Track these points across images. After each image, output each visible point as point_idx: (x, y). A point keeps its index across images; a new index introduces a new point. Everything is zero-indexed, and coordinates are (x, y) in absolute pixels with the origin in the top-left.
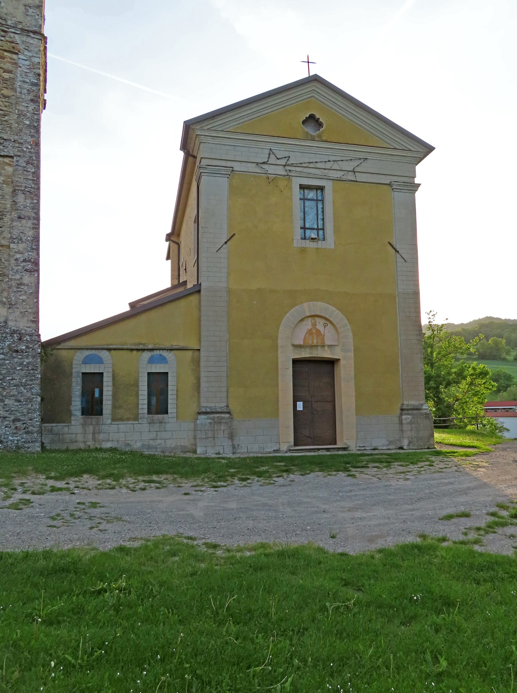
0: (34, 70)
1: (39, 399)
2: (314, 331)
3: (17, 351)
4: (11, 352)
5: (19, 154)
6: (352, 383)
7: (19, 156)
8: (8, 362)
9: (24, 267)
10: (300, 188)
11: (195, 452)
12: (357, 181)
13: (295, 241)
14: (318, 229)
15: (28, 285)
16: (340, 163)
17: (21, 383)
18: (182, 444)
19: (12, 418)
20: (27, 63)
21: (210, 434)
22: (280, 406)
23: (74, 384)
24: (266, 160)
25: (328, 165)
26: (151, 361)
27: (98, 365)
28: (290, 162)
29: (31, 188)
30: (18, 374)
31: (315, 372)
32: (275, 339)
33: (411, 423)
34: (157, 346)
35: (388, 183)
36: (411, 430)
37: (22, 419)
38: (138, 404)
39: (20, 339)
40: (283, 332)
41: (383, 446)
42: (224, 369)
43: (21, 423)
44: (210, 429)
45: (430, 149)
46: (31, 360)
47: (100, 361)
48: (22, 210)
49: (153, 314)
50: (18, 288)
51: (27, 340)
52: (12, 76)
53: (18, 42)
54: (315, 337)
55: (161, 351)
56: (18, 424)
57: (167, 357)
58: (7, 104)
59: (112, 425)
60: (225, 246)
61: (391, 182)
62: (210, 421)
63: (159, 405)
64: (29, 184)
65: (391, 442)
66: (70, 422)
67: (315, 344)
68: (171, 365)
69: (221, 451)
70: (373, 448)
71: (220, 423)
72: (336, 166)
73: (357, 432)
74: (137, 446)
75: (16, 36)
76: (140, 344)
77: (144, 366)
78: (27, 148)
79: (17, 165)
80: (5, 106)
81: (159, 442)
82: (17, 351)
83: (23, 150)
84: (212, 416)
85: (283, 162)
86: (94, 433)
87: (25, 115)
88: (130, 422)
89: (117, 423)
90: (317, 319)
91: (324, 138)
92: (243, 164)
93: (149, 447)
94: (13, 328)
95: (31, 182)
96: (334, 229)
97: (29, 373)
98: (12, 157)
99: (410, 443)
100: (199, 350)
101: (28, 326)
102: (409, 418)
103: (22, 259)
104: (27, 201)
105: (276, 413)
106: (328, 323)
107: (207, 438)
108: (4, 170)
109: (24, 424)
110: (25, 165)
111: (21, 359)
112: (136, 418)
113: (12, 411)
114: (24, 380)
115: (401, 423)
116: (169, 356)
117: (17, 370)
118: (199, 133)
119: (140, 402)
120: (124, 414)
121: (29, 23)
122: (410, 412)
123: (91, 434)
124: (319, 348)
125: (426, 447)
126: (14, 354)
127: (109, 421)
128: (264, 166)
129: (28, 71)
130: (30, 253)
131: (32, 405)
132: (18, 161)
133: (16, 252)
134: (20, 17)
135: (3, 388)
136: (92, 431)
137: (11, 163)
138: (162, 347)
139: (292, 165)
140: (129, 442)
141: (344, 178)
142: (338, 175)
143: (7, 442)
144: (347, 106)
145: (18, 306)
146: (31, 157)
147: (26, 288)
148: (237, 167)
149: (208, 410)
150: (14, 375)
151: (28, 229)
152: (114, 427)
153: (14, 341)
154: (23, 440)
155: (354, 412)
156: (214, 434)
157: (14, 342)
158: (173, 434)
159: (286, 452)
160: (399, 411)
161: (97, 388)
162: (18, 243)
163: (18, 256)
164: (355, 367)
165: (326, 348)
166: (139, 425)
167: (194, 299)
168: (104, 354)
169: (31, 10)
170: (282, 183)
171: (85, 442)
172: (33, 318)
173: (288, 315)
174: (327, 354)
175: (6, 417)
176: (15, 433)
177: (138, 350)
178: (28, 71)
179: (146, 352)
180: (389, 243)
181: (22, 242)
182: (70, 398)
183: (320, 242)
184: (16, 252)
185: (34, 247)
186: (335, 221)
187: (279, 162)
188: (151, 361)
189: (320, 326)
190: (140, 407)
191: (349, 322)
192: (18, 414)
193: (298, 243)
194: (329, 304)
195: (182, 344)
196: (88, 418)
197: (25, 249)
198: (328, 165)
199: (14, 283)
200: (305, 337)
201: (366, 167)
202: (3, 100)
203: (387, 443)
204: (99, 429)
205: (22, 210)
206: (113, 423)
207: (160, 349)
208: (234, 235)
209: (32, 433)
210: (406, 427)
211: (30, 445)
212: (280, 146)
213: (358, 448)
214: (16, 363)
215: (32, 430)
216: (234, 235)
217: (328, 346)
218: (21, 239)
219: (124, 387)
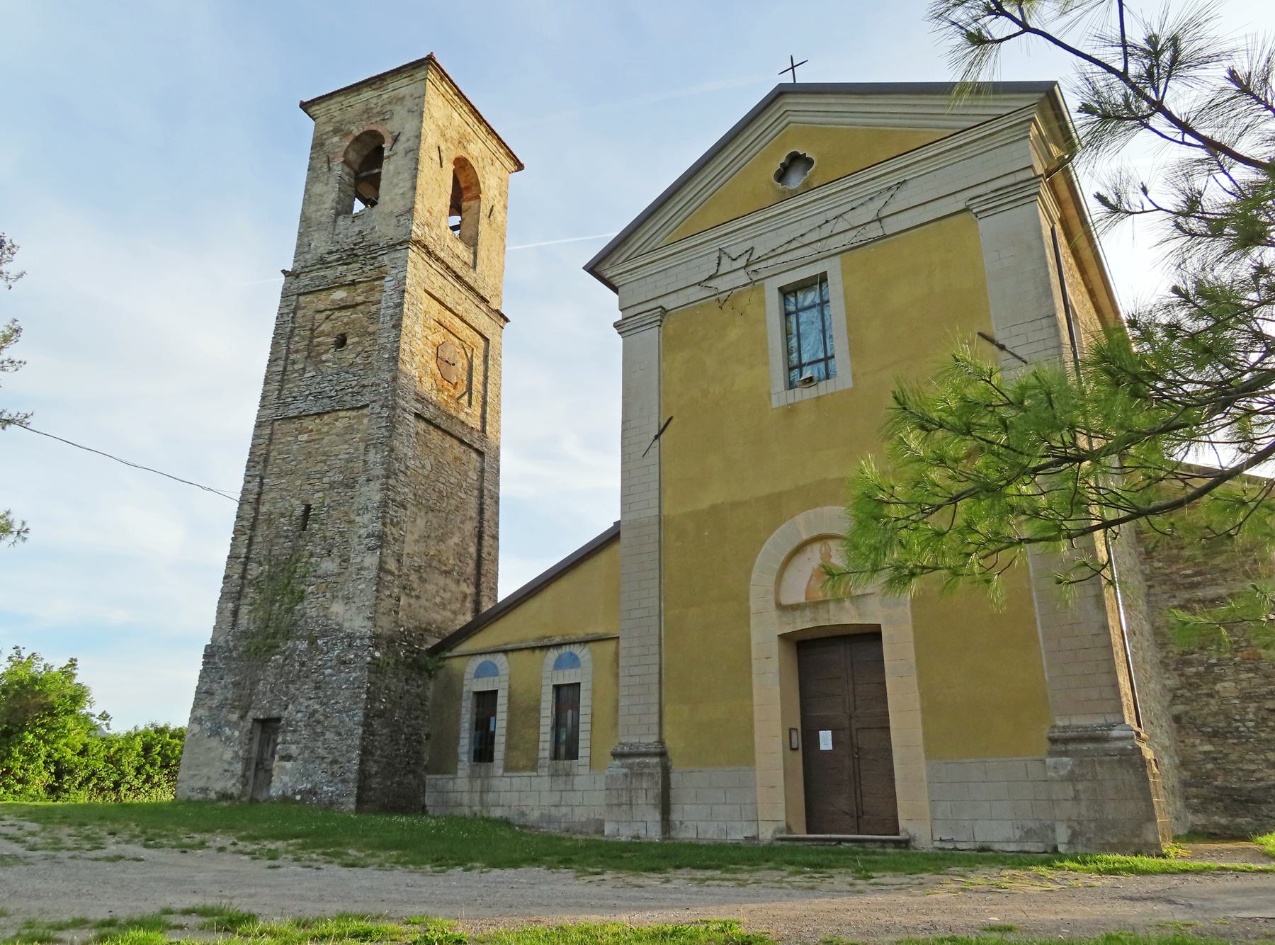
1: (360, 731)
3: (344, 663)
6: (913, 679)
13: (774, 397)
21: (624, 799)
23: (463, 711)
25: (825, 231)
26: (559, 665)
31: (833, 661)
32: (742, 599)
35: (962, 206)
36: (1076, 798)
39: (350, 645)
41: (1008, 841)
56: (336, 768)
62: (625, 770)
65: (1028, 834)
66: (456, 773)
68: (585, 670)
70: (978, 845)
71: (641, 774)
74: (534, 815)
77: (548, 673)
81: (564, 810)
82: (344, 663)
85: (742, 262)
86: (481, 792)
93: (550, 820)
96: (850, 348)
102: (1064, 765)
105: (747, 757)
107: (619, 805)
112: (534, 767)
116: (583, 653)
120: (524, 761)
122: (1071, 747)
127: (500, 772)
128: (712, 283)
138: (574, 638)
139: (759, 260)
144: (849, 104)
148: (669, 303)
149: (626, 749)
155: (921, 751)
156: (631, 798)
157: (342, 651)
158: (586, 796)
163: (362, 531)
165: (847, 604)
168: (500, 660)
173: (766, 546)
177: (542, 648)
182: (458, 732)
183: (822, 384)
186: (850, 331)
187: (737, 265)
188: (559, 665)
193: (780, 396)
195: (600, 630)
201: (904, 198)
203: (1018, 833)
207: (570, 644)
208: (670, 419)
216: (670, 419)
219: (524, 713)
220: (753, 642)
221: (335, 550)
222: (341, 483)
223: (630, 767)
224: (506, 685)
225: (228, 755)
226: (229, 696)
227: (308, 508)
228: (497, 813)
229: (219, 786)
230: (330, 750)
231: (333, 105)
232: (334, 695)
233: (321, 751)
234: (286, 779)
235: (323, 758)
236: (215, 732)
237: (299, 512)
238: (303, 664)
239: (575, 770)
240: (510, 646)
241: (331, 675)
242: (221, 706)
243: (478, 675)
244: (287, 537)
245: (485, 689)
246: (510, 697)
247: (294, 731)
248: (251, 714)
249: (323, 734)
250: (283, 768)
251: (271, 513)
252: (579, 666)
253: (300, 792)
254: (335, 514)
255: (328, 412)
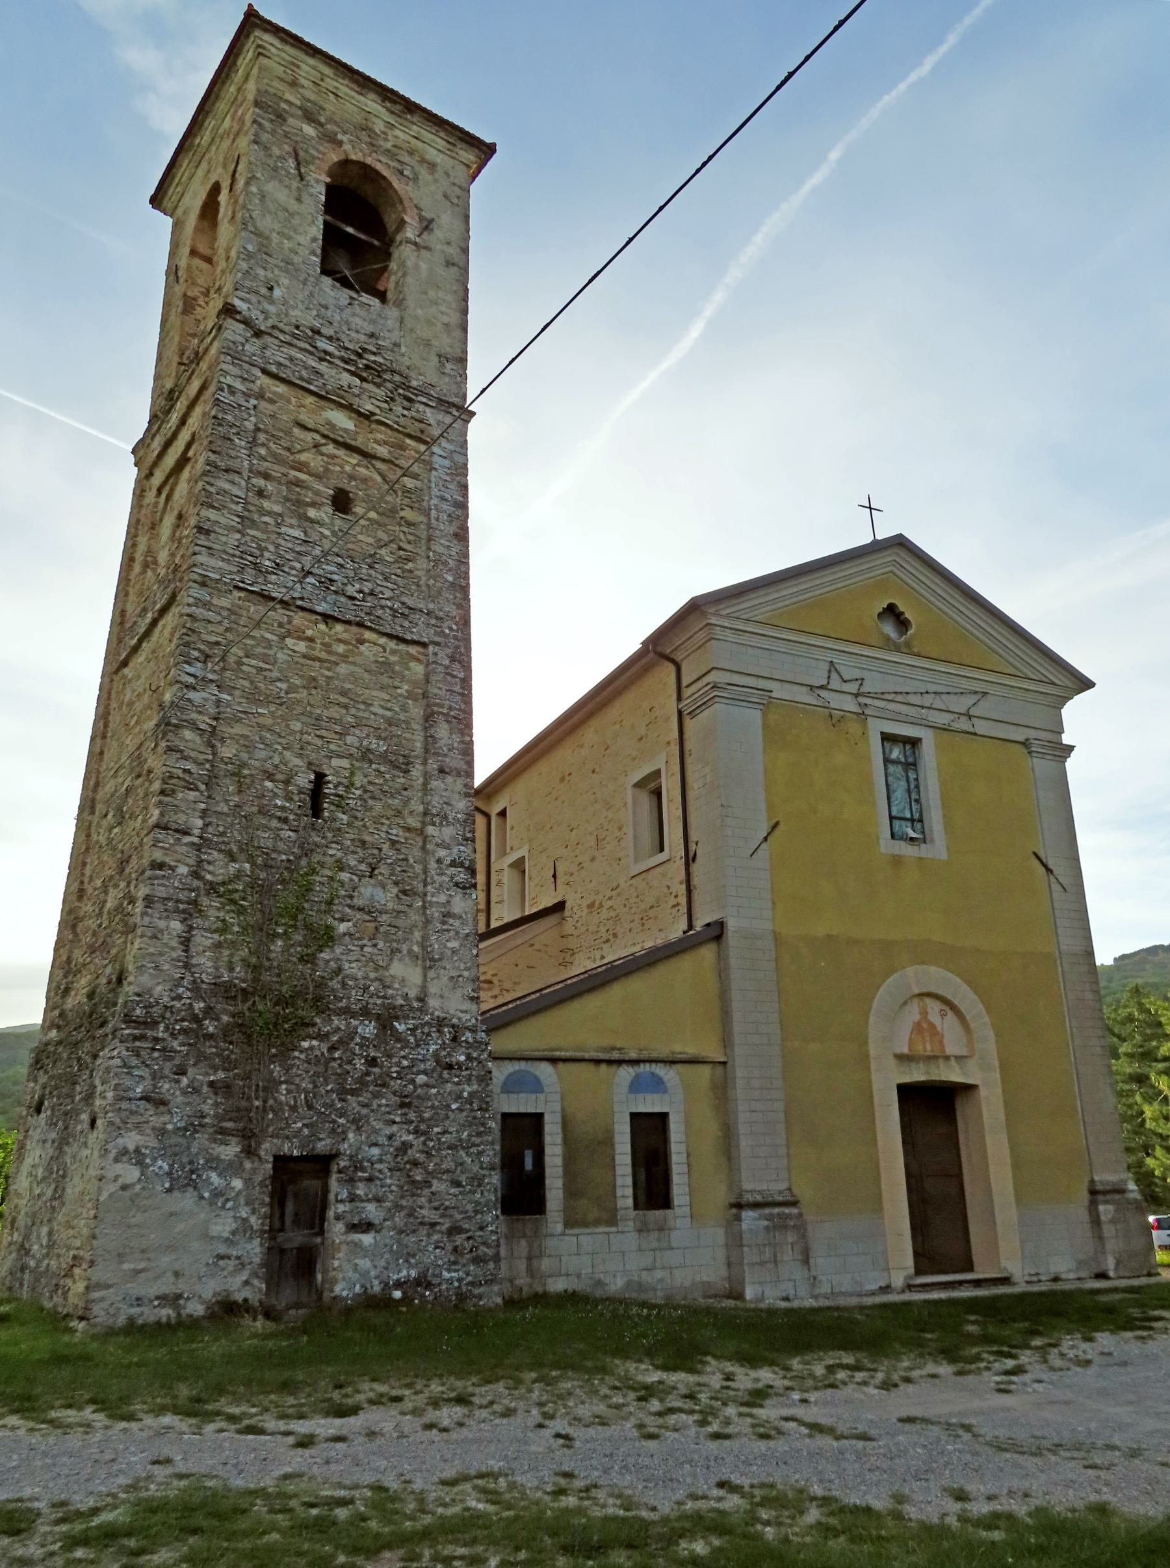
0: (458, 479)
2: (925, 1026)
4: (439, 1069)
5: (437, 639)
6: (1004, 1137)
7: (438, 644)
8: (434, 1091)
9: (452, 878)
10: (883, 740)
11: (740, 1296)
12: (975, 734)
14: (912, 820)
15: (461, 917)
16: (944, 697)
17: (460, 1140)
18: (705, 1279)
19: (447, 1226)
20: (447, 463)
21: (768, 1255)
22: (883, 1187)
24: (824, 682)
25: (927, 700)
26: (636, 1087)
27: (533, 1096)
28: (864, 689)
29: (460, 710)
30: (454, 1121)
33: (1113, 1221)
34: (645, 1055)
37: (466, 1226)
38: (614, 1186)
39: (454, 1039)
40: (875, 1031)
42: (780, 1106)
43: (464, 1236)
44: (766, 1242)
45: (1086, 684)
46: (475, 1087)
47: (536, 1086)
48: (446, 755)
49: (635, 984)
50: (444, 923)
51: (466, 1042)
52: (418, 484)
53: (432, 422)
54: (928, 1039)
55: (654, 1065)
56: (459, 1240)
57: (665, 1079)
58: (411, 538)
59: (566, 1238)
60: (764, 846)
61: (1027, 740)
63: (654, 1190)
64: (456, 703)
67: (929, 1053)
68: (677, 1099)
69: (792, 1293)
72: (938, 704)
73: (1022, 1242)
74: (616, 1285)
75: (428, 410)
76: (614, 1049)
77: (620, 1100)
78: (451, 629)
79: (434, 662)
80: (409, 543)
81: (659, 1274)
82: (450, 1067)
83: (443, 632)
84: (767, 1211)
85: (853, 688)
86: (529, 1259)
87: (445, 563)
88: (600, 1229)
89: (576, 1231)
90: (928, 1000)
91: (915, 650)
92: (787, 686)
93: (641, 1287)
94: (437, 1013)
95: (458, 698)
97: (475, 1118)
98: (424, 645)
99: (1118, 1263)
100: (724, 1063)
101: (464, 1008)
103: (449, 859)
104: (454, 736)
105: (876, 1203)
106: (947, 1009)
108: (409, 669)
109: (469, 1238)
110: (447, 662)
111: (458, 1084)
113: (446, 1208)
114: (466, 1134)
115: (1096, 1221)
116: (668, 1074)
117: (453, 1111)
118: (713, 620)
119: (619, 1181)
121: (443, 386)
122: (1109, 1197)
123: (524, 1261)
124: (941, 1061)
125: (1145, 1272)
126: (445, 1074)
127: (559, 1228)
128: (823, 693)
129: (448, 478)
130: (462, 848)
131: (482, 1193)
132: (435, 654)
133: (437, 845)
134: (432, 376)
135: (427, 1153)
136: (524, 1253)
137: (421, 657)
138: (654, 1055)
139: (867, 695)
140: (602, 1276)
141: (956, 726)
142: (943, 719)
143: (440, 1284)
145: (444, 963)
146: (457, 647)
147: (457, 923)
148: (779, 691)
149: (759, 1198)
150: (447, 1123)
151: (457, 796)
152: (569, 1243)
153: (444, 1043)
154: (470, 1278)
155: (1012, 1198)
158: (683, 1256)
159: (903, 1291)
160: (1085, 1196)
161: (529, 1148)
162: (441, 825)
163: (442, 853)
164: (1006, 1104)
165: (953, 1062)
166: (619, 1236)
167: (707, 953)
168: (544, 1070)
169: (449, 366)
170: (854, 727)
171: (511, 1281)
172: (473, 990)
174: (953, 1075)
175: (435, 1224)
176: (455, 1263)
177: (610, 1062)
178: (448, 478)
179: (625, 1066)
180: (1035, 854)
181: (448, 824)
184: (437, 845)
185: (469, 835)
186: (944, 806)
188: (636, 1087)
189: (934, 1018)
190: (619, 1193)
191: (987, 1009)
192: (458, 1217)
194: (949, 970)
195: (691, 1050)
196: (518, 1220)
197: (453, 838)
198: (927, 700)
199: (434, 912)
200: (910, 1039)
202: (406, 530)
204: (540, 1246)
205: (446, 755)
206: (567, 1232)
209: (486, 1262)
210: (1108, 1230)
211: (482, 1289)
212: (846, 657)
213: (1027, 1278)
214: (450, 1093)
215: (485, 1254)
217: (957, 1057)
218: (445, 817)
219: (586, 1149)
220: (875, 1087)
221: (383, 869)
222: (384, 757)
223: (769, 1218)
224: (558, 1107)
225: (223, 1226)
226: (208, 1108)
227: (320, 779)
228: (558, 1285)
229: (210, 1289)
230: (445, 1211)
231: (308, 67)
232: (435, 1120)
233: (427, 1213)
234: (364, 1263)
235: (433, 1225)
236: (186, 1179)
237: (304, 780)
238: (372, 1062)
239: (671, 1223)
240: (562, 1054)
241: (427, 1085)
242: (192, 1128)
243: (507, 1088)
244: (285, 820)
245: (522, 1110)
246: (565, 1123)
247: (370, 1180)
248: (267, 1148)
249: (428, 1184)
250: (357, 1245)
251: (243, 765)
252: (665, 1091)
253: (398, 1285)
254: (378, 808)
255: (348, 622)
